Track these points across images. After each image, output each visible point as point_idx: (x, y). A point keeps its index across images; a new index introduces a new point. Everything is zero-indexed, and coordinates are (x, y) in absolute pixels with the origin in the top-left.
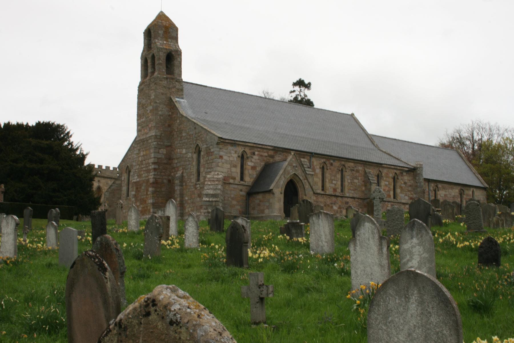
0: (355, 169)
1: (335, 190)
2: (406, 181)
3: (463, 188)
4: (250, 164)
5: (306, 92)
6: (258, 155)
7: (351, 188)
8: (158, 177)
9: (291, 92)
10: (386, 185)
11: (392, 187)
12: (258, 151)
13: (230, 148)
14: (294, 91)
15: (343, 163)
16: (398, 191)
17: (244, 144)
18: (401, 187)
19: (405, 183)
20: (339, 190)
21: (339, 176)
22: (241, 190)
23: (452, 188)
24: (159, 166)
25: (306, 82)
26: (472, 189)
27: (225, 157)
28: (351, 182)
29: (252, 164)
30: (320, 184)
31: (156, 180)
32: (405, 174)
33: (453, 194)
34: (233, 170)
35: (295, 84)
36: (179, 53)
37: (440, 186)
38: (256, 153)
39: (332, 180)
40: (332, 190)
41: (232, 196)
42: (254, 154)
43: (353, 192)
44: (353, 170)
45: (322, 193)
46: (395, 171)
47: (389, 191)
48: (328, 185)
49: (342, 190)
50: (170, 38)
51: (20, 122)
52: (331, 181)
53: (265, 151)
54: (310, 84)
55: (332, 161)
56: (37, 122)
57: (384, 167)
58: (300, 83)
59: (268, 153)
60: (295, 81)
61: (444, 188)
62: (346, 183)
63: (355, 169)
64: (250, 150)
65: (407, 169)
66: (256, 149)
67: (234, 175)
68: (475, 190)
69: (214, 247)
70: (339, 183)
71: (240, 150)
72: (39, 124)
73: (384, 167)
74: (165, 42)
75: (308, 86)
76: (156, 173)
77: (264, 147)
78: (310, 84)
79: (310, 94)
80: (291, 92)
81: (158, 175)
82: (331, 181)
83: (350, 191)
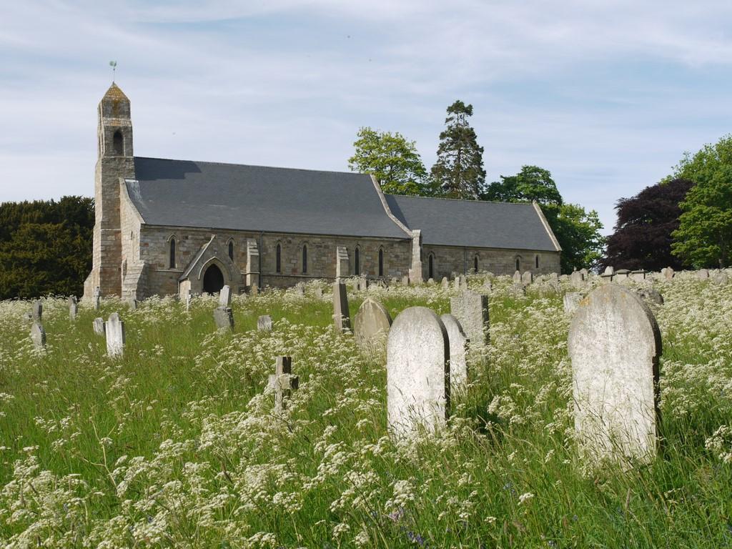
0: (323, 245)
1: (294, 270)
2: (399, 254)
3: (520, 254)
4: (181, 249)
5: (467, 118)
6: (192, 238)
7: (317, 267)
8: (107, 265)
9: (447, 120)
10: (368, 261)
11: (377, 262)
12: (192, 235)
13: (157, 234)
14: (451, 119)
15: (306, 239)
16: (385, 266)
17: (175, 228)
18: (391, 263)
19: (397, 256)
20: (301, 270)
21: (300, 254)
22: (171, 278)
23: (503, 256)
24: (107, 254)
25: (466, 105)
26: (535, 255)
27: (151, 245)
28: (317, 260)
29: (185, 249)
30: (275, 265)
31: (104, 270)
32: (396, 245)
33: (505, 262)
34: (162, 256)
35: (450, 110)
36: (129, 130)
37: (483, 253)
38: (190, 237)
39: (291, 260)
40: (290, 270)
41: (160, 284)
42: (187, 238)
43: (320, 271)
44: (321, 247)
45: (277, 274)
46: (382, 243)
47: (372, 267)
48: (284, 264)
49: (305, 271)
50: (120, 113)
51: (38, 200)
52: (289, 261)
53: (201, 233)
54: (470, 107)
55: (290, 239)
56: (63, 197)
57: (364, 240)
58: (458, 107)
59: (203, 235)
60: (451, 105)
61: (489, 256)
62: (309, 262)
63: (323, 245)
64: (182, 234)
65: (398, 240)
66: (189, 232)
67: (162, 262)
68: (540, 255)
69: (200, 335)
70: (301, 262)
71: (169, 236)
72: (65, 199)
73: (364, 240)
74: (114, 119)
75: (468, 111)
76: (104, 262)
77: (198, 229)
78: (470, 107)
79: (473, 122)
80: (447, 120)
81: (106, 263)
82: (289, 261)
83: (315, 270)
